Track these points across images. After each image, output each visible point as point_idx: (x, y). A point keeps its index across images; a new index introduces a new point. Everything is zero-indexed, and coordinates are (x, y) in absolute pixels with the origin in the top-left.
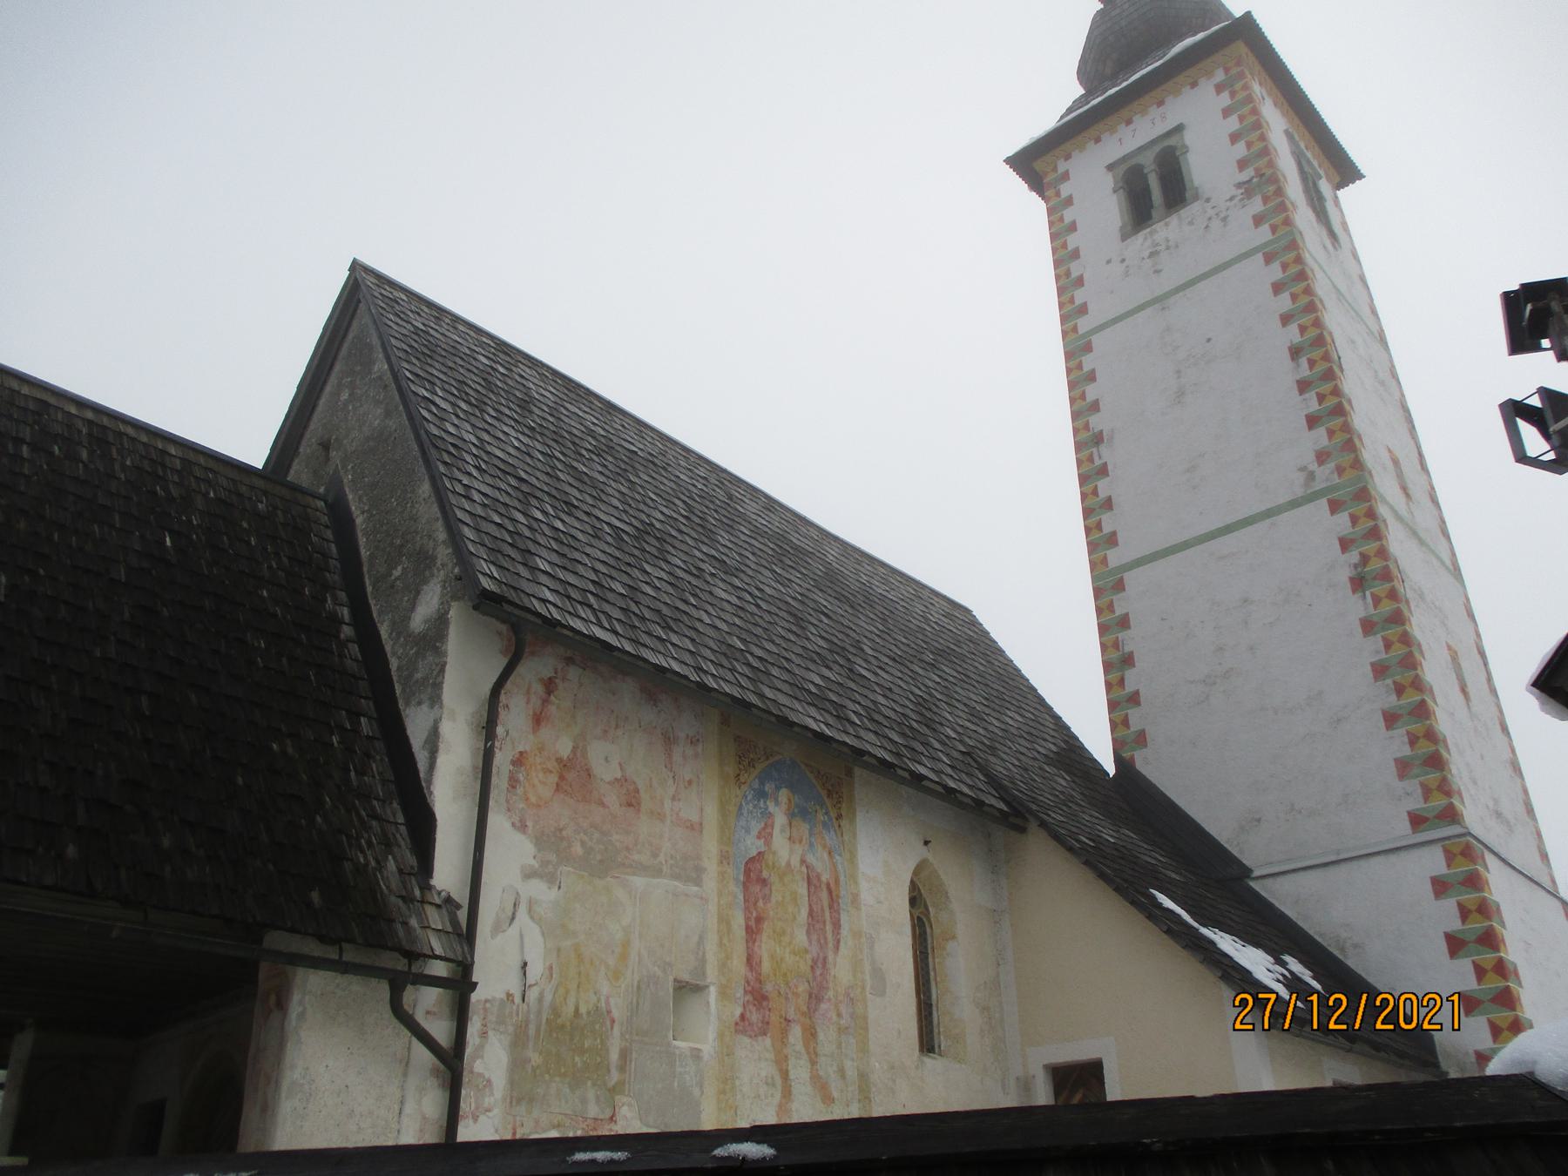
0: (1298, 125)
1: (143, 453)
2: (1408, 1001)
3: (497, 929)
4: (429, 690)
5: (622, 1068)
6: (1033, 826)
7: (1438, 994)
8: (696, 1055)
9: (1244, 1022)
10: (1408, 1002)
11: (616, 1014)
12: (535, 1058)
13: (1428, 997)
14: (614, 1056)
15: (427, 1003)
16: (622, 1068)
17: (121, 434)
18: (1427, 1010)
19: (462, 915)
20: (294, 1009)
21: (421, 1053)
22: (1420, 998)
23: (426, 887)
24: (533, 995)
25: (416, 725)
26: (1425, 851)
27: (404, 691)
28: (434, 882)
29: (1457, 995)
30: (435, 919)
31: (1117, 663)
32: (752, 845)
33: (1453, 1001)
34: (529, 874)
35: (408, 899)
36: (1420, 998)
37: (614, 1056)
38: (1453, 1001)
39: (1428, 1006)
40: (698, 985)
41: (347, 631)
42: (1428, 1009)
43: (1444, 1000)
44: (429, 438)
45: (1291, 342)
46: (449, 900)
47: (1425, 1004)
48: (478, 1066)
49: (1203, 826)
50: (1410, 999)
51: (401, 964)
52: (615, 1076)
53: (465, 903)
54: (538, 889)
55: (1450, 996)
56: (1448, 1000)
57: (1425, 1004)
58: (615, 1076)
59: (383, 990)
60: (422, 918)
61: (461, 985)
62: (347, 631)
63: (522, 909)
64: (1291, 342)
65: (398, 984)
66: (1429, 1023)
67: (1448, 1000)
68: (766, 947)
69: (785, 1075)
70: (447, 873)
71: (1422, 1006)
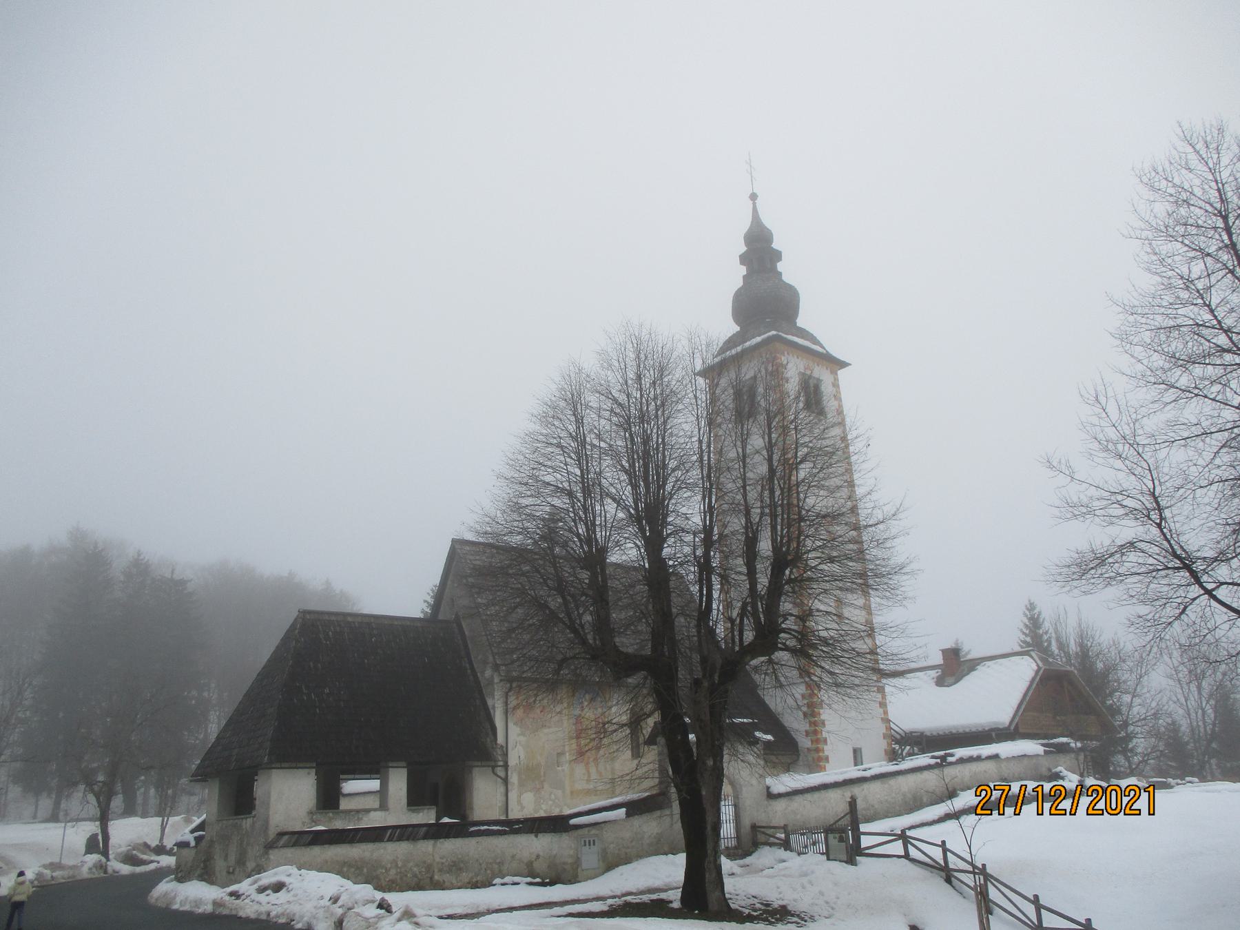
3: (513, 749)
5: (545, 776)
6: (1043, 754)
8: (563, 770)
10: (1114, 792)
11: (542, 764)
12: (524, 777)
14: (542, 773)
15: (501, 773)
16: (545, 776)
17: (710, 390)
19: (505, 749)
20: (474, 775)
21: (499, 779)
22: (1123, 790)
23: (496, 744)
24: (522, 763)
25: (490, 702)
28: (498, 742)
29: (1152, 787)
30: (499, 752)
32: (577, 712)
34: (519, 735)
35: (493, 748)
36: (1123, 790)
37: (542, 773)
38: (1149, 792)
41: (469, 671)
42: (1129, 798)
46: (502, 746)
47: (1127, 794)
48: (511, 780)
51: (493, 764)
52: (542, 778)
53: (505, 746)
54: (522, 738)
57: (1127, 794)
58: (542, 778)
59: (490, 768)
60: (496, 752)
61: (506, 766)
62: (469, 671)
63: (518, 744)
65: (493, 767)
66: (1130, 809)
67: (1145, 791)
69: (588, 772)
70: (500, 739)
71: (1125, 796)
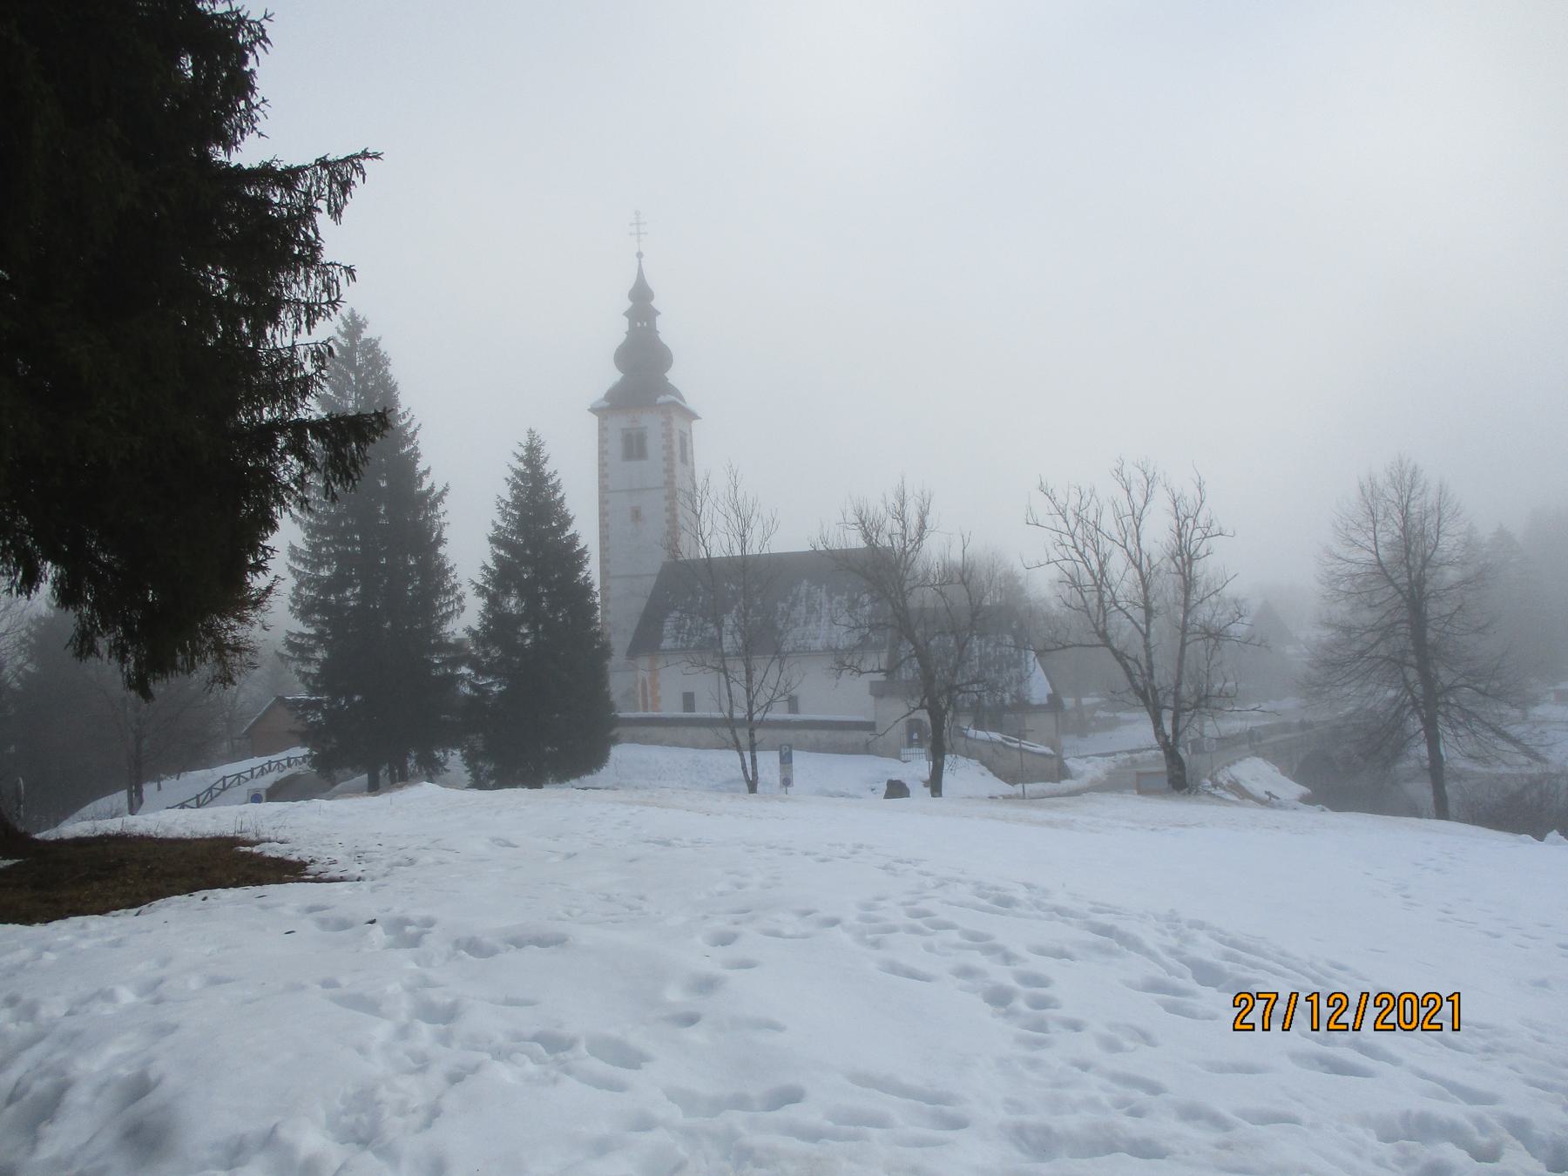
0: (263, 611)
7: (1414, 994)
9: (1244, 1022)
13: (1428, 997)
22: (1420, 998)
27: (251, 718)
33: (1312, 1001)
36: (1420, 998)
39: (1428, 1006)
42: (1427, 1009)
43: (1444, 1000)
44: (720, 699)
47: (1425, 1003)
49: (110, 797)
50: (1410, 999)
55: (1310, 996)
56: (1447, 1000)
57: (1425, 1003)
67: (1447, 1000)
68: (788, 931)
71: (1422, 1006)
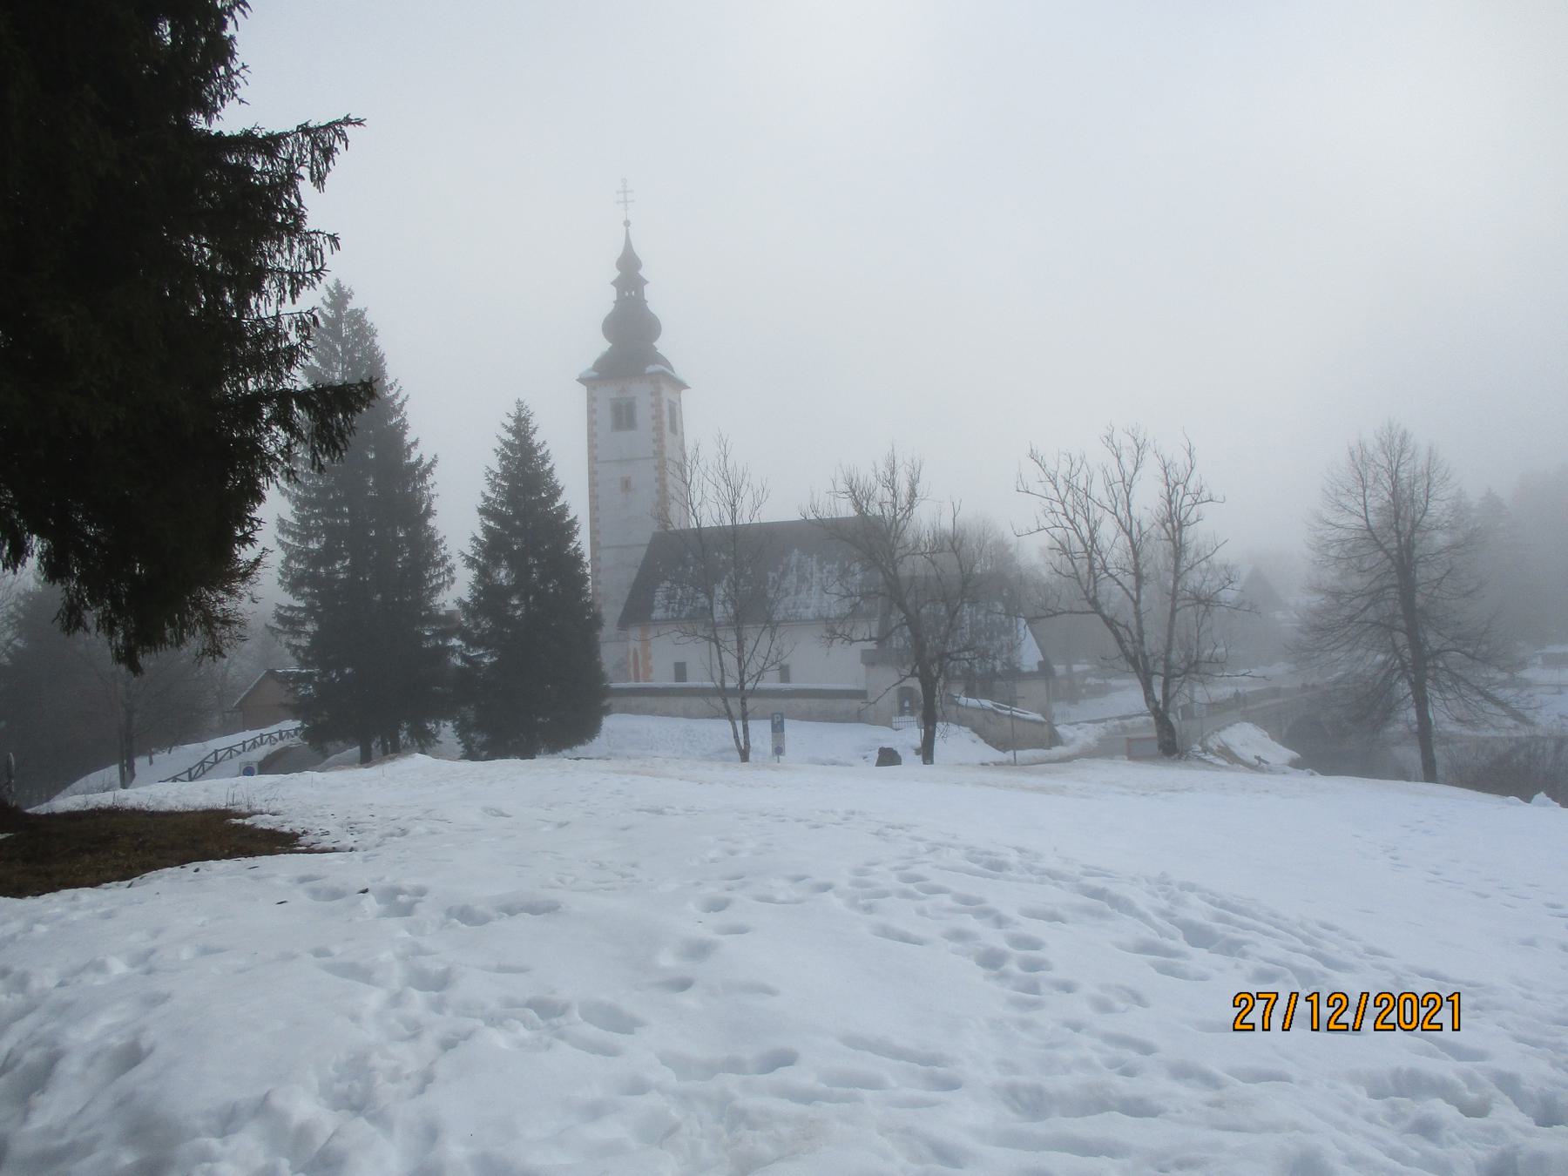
1: (969, 585)
2: (1408, 1001)
4: (801, 610)
7: (1345, 995)
18: (1427, 1010)
22: (1420, 998)
26: (752, 733)
31: (593, 497)
33: (1312, 1001)
36: (1420, 998)
38: (1453, 1001)
40: (1325, 966)
43: (1444, 999)
45: (1116, 615)
47: (1425, 1004)
50: (1410, 999)
55: (1450, 996)
56: (1448, 1000)
57: (1425, 1004)
64: (1116, 615)
66: (1429, 1024)
67: (1448, 1000)
71: (1422, 1006)
